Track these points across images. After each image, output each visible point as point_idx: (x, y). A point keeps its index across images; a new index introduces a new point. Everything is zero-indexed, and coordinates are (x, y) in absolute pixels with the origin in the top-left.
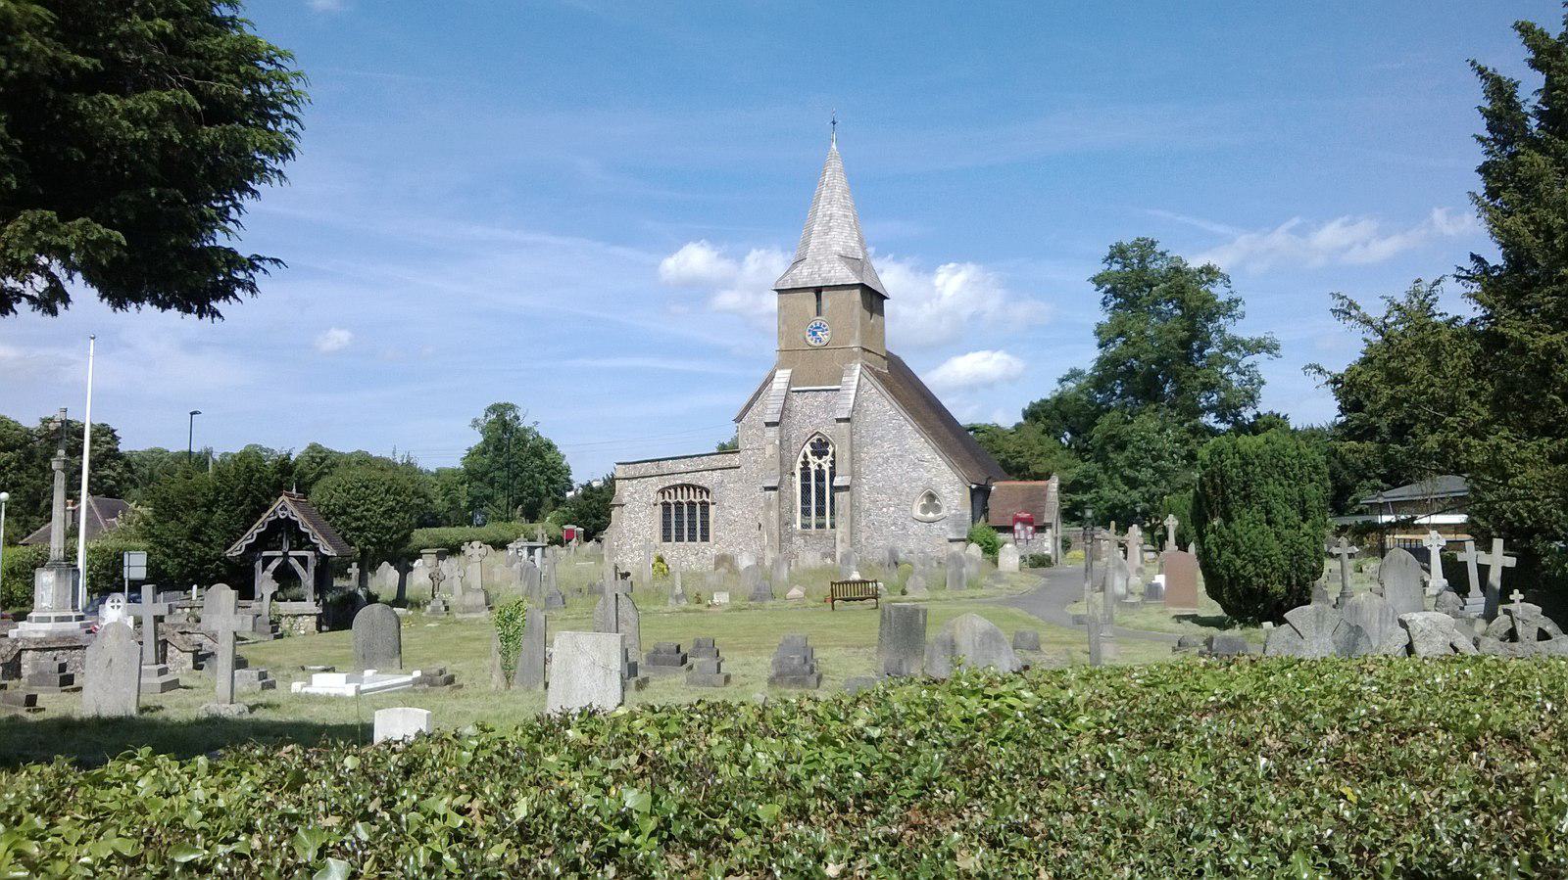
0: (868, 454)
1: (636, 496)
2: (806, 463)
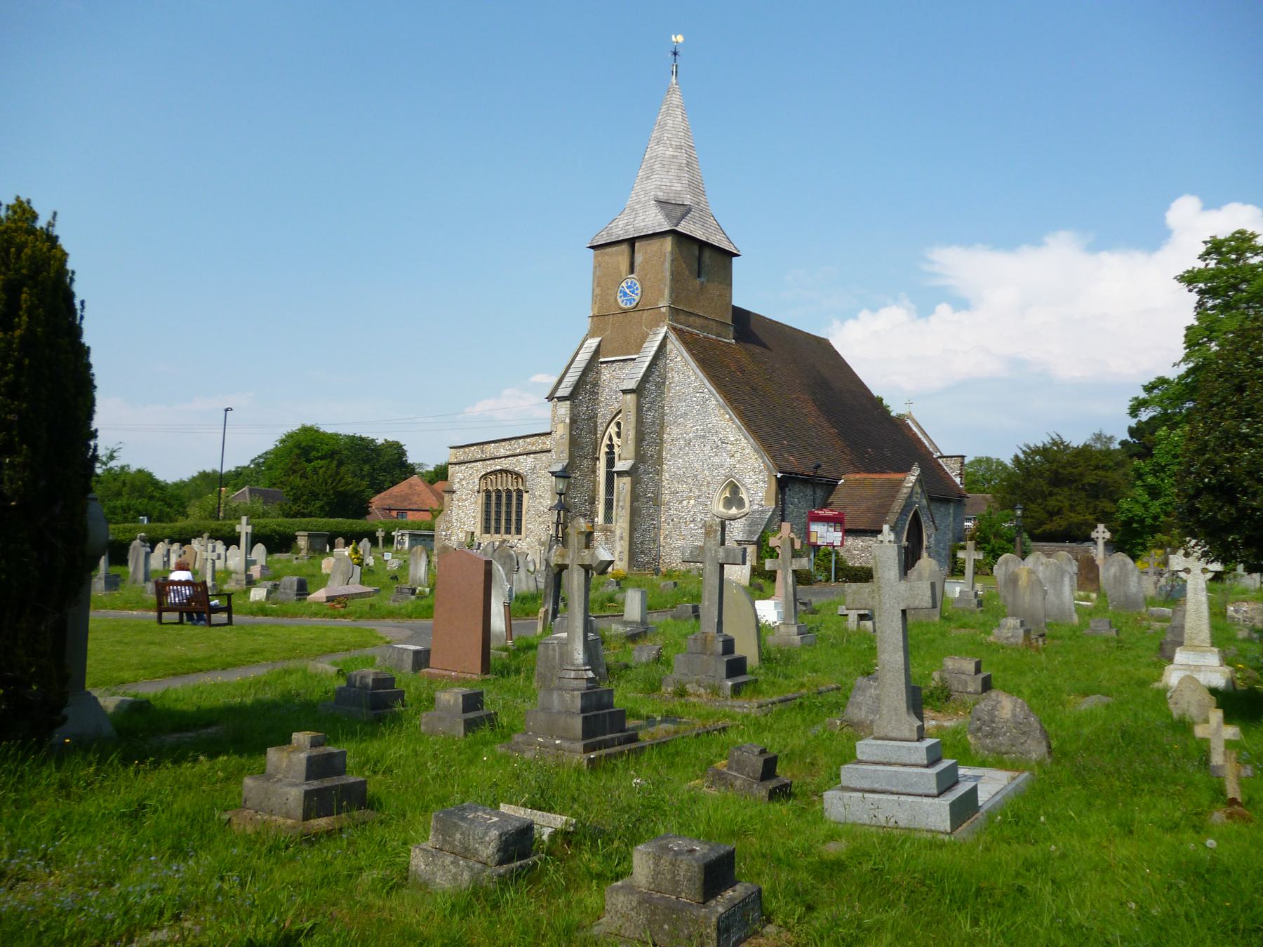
0: (672, 434)
1: (464, 483)
2: (611, 447)
